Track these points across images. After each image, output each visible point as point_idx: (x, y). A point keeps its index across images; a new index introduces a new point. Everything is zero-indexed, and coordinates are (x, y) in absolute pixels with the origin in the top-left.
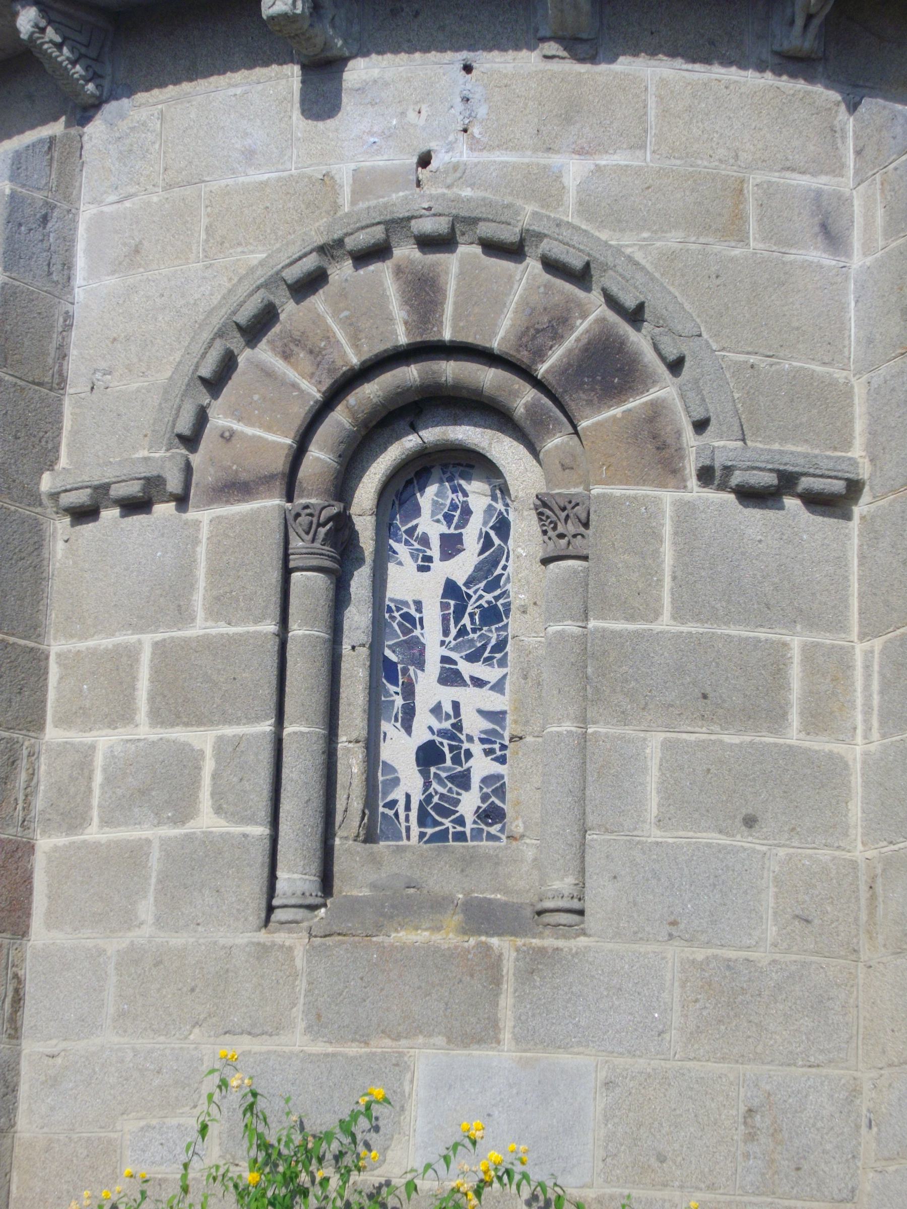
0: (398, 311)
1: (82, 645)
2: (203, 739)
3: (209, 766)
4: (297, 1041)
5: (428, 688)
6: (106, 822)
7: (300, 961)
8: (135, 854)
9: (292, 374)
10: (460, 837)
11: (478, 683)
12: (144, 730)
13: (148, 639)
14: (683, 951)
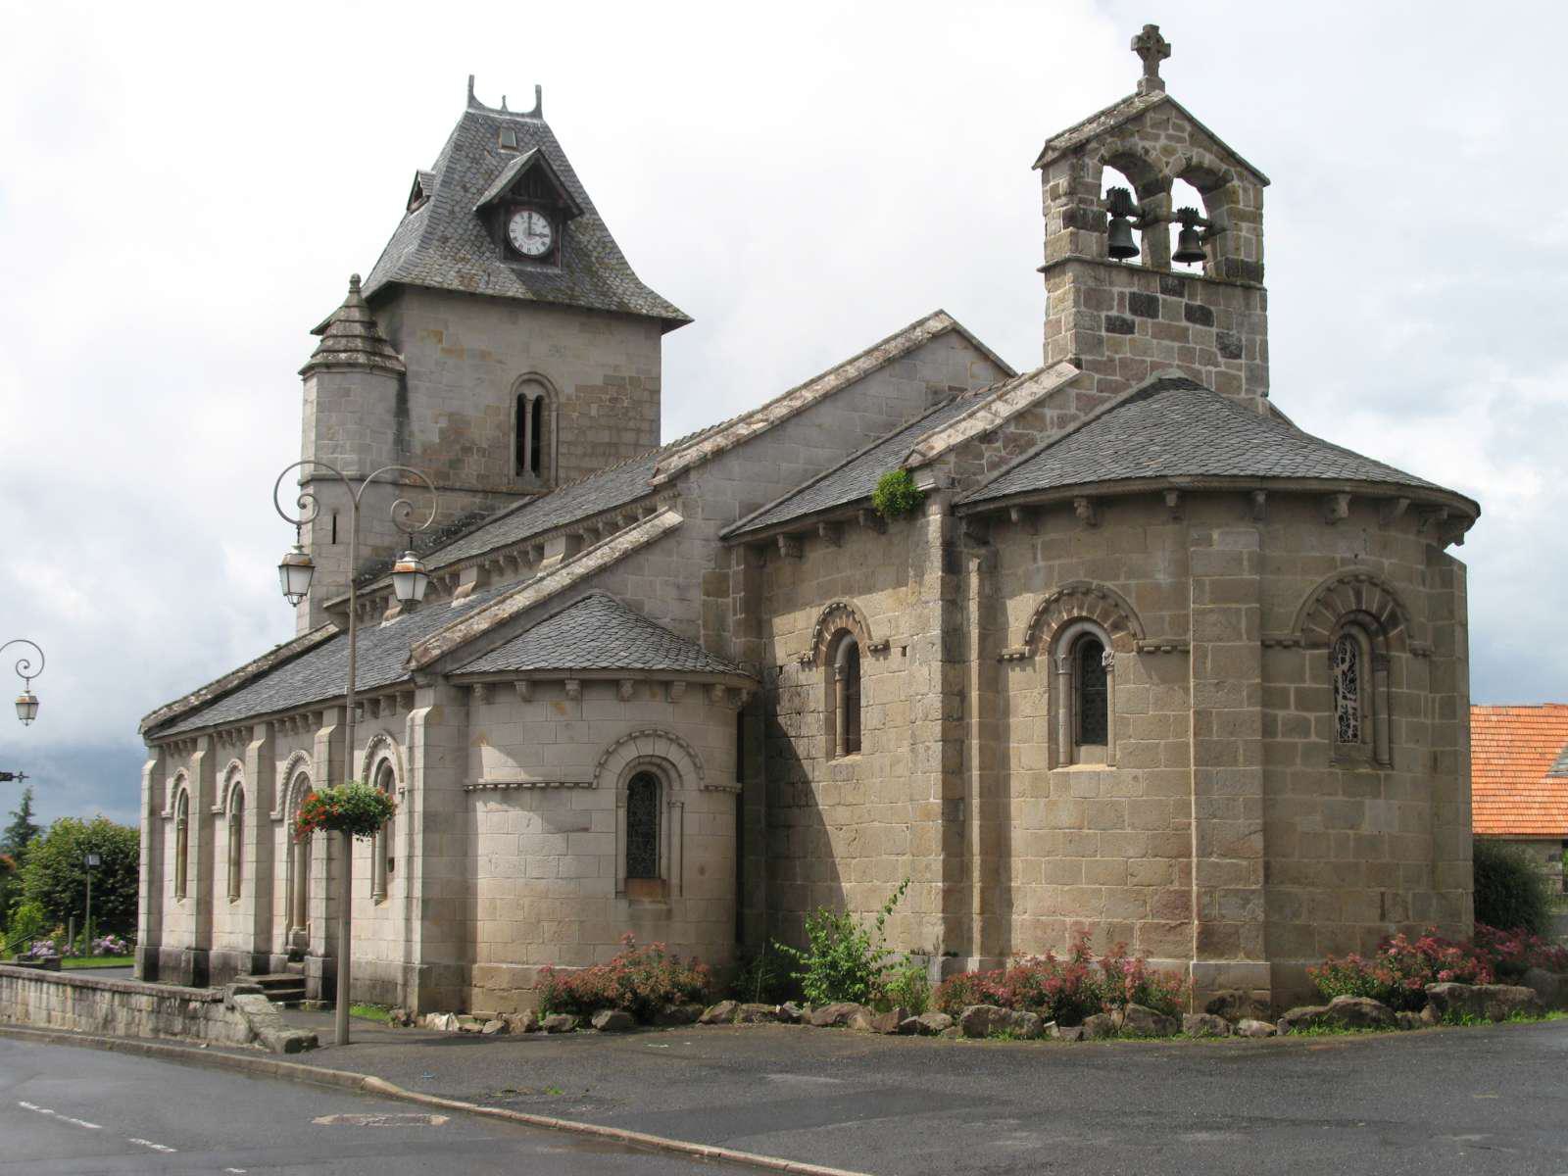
0: (1353, 599)
2: (1311, 716)
4: (1340, 798)
6: (1283, 736)
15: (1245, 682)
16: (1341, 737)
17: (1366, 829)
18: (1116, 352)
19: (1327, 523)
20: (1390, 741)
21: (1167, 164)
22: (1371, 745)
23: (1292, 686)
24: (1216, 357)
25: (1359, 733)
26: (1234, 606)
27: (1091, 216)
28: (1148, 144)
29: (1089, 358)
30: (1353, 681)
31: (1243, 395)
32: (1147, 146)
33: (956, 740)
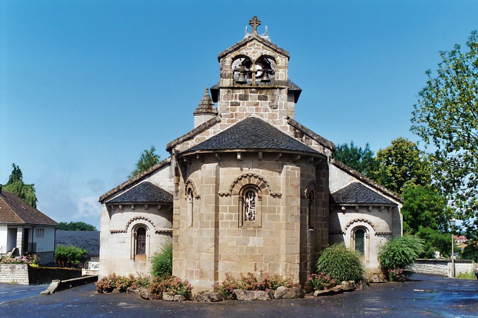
2: (233, 214)
3: (234, 216)
4: (241, 237)
5: (249, 209)
8: (228, 223)
12: (228, 213)
13: (228, 206)
17: (250, 245)
18: (234, 111)
21: (254, 56)
26: (209, 185)
28: (247, 51)
29: (224, 114)
30: (254, 203)
31: (278, 119)
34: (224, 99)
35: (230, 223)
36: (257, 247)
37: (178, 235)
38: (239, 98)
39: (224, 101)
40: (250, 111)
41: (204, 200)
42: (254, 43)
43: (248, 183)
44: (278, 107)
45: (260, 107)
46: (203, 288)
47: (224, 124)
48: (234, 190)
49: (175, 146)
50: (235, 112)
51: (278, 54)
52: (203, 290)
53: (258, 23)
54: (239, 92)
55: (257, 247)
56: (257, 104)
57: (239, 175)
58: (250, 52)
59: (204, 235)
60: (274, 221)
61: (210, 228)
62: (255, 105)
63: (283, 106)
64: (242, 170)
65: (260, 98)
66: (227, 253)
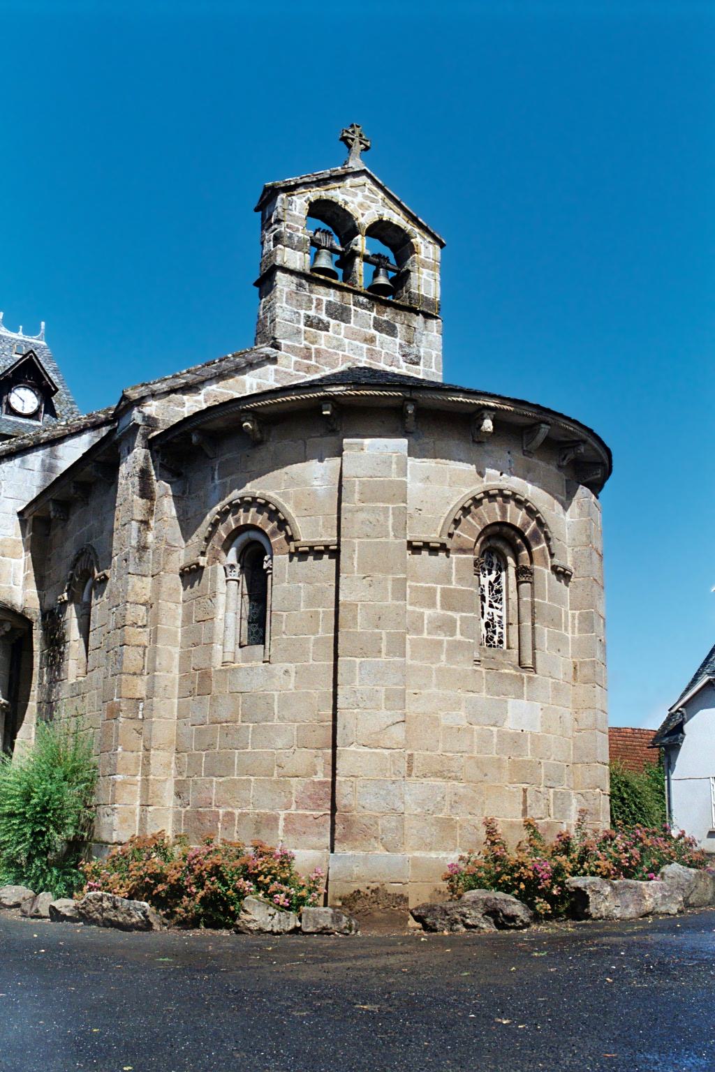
1: (418, 584)
2: (457, 616)
3: (458, 623)
4: (484, 694)
7: (484, 675)
8: (440, 643)
9: (474, 523)
10: (494, 646)
11: (497, 608)
12: (439, 611)
13: (439, 587)
14: (78, 693)
15: (390, 577)
16: (487, 642)
17: (510, 725)
18: (312, 343)
19: (474, 441)
20: (534, 648)
21: (363, 215)
22: (516, 651)
23: (454, 585)
24: (398, 361)
25: (504, 640)
26: (382, 505)
27: (296, 239)
28: (348, 199)
29: (289, 343)
32: (347, 200)
33: (138, 646)
34: (287, 302)
35: (445, 645)
36: (526, 735)
37: (138, 696)
38: (327, 309)
39: (286, 306)
40: (354, 354)
41: (356, 556)
42: (362, 182)
43: (499, 520)
44: (421, 363)
45: (378, 349)
46: (359, 879)
47: (287, 370)
48: (459, 536)
49: (141, 401)
50: (316, 346)
51: (417, 230)
52: (356, 886)
53: (364, 142)
54: (327, 295)
55: (526, 735)
56: (371, 340)
57: (477, 489)
58: (353, 203)
59: (357, 683)
60: (561, 653)
61: (383, 658)
62: (366, 340)
63: (433, 360)
64: (481, 474)
65: (378, 325)
66: (439, 752)
